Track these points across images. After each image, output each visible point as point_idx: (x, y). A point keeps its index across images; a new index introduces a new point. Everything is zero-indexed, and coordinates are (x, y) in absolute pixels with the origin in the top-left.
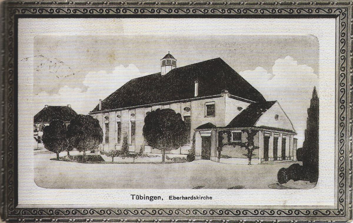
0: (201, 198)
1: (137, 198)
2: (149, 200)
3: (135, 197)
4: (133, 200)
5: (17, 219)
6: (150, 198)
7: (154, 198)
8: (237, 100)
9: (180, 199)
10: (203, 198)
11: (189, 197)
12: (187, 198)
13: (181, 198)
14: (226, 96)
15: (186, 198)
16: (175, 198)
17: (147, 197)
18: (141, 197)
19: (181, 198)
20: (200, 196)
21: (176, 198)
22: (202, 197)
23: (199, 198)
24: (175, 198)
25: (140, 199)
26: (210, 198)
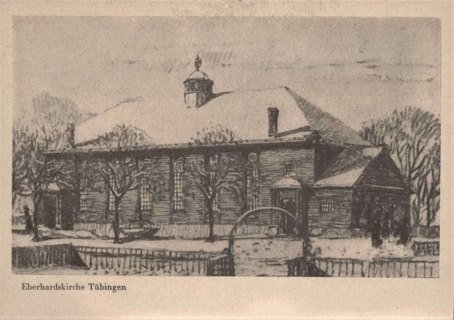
0: (69, 288)
1: (97, 288)
2: (112, 290)
3: (93, 287)
4: (91, 291)
5: (402, 189)
6: (112, 288)
7: (118, 288)
8: (249, 277)
9: (38, 289)
10: (72, 288)
11: (51, 287)
12: (48, 287)
13: (40, 288)
14: (43, 225)
15: (47, 288)
16: (30, 288)
17: (108, 287)
18: (101, 286)
19: (40, 288)
20: (67, 284)
21: (31, 288)
22: (70, 287)
23: (66, 288)
24: (30, 288)
25: (101, 289)
26: (82, 288)
